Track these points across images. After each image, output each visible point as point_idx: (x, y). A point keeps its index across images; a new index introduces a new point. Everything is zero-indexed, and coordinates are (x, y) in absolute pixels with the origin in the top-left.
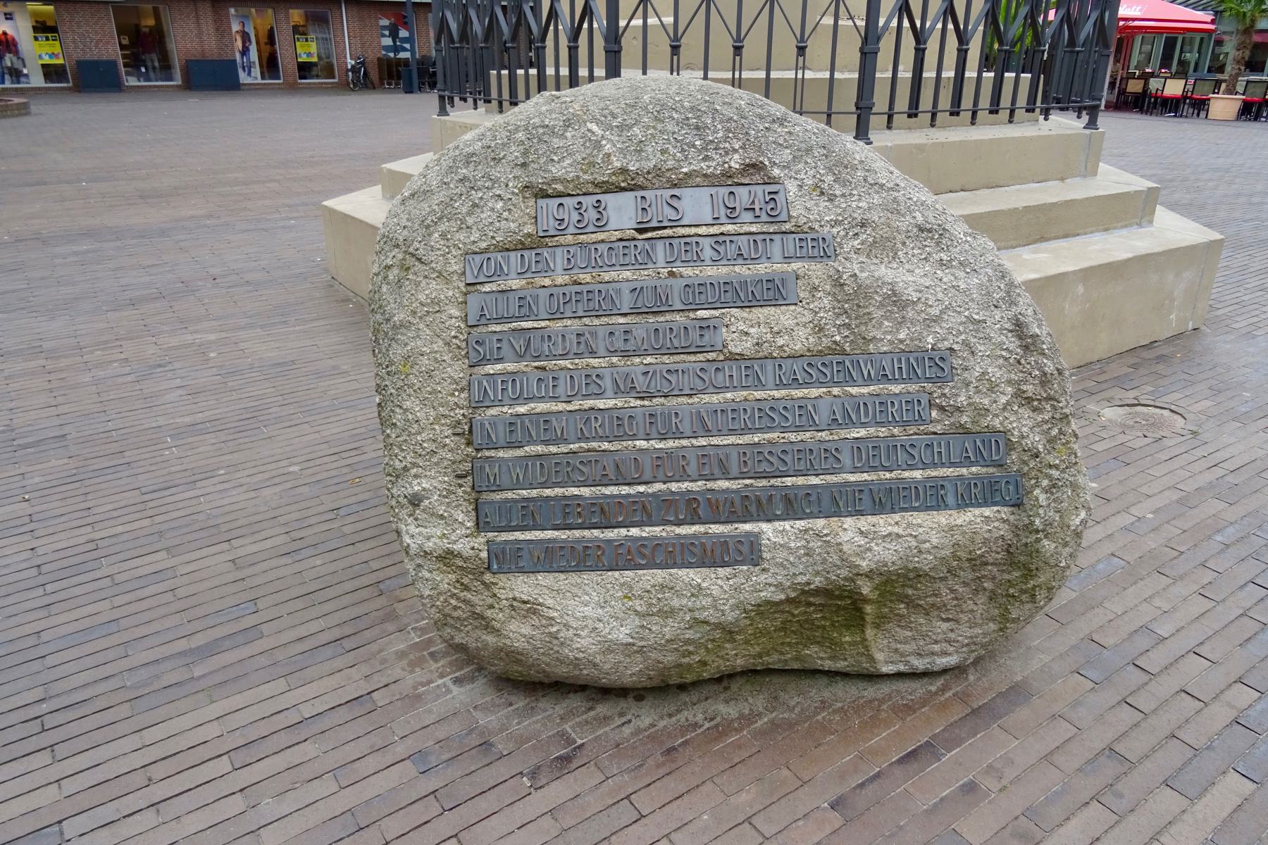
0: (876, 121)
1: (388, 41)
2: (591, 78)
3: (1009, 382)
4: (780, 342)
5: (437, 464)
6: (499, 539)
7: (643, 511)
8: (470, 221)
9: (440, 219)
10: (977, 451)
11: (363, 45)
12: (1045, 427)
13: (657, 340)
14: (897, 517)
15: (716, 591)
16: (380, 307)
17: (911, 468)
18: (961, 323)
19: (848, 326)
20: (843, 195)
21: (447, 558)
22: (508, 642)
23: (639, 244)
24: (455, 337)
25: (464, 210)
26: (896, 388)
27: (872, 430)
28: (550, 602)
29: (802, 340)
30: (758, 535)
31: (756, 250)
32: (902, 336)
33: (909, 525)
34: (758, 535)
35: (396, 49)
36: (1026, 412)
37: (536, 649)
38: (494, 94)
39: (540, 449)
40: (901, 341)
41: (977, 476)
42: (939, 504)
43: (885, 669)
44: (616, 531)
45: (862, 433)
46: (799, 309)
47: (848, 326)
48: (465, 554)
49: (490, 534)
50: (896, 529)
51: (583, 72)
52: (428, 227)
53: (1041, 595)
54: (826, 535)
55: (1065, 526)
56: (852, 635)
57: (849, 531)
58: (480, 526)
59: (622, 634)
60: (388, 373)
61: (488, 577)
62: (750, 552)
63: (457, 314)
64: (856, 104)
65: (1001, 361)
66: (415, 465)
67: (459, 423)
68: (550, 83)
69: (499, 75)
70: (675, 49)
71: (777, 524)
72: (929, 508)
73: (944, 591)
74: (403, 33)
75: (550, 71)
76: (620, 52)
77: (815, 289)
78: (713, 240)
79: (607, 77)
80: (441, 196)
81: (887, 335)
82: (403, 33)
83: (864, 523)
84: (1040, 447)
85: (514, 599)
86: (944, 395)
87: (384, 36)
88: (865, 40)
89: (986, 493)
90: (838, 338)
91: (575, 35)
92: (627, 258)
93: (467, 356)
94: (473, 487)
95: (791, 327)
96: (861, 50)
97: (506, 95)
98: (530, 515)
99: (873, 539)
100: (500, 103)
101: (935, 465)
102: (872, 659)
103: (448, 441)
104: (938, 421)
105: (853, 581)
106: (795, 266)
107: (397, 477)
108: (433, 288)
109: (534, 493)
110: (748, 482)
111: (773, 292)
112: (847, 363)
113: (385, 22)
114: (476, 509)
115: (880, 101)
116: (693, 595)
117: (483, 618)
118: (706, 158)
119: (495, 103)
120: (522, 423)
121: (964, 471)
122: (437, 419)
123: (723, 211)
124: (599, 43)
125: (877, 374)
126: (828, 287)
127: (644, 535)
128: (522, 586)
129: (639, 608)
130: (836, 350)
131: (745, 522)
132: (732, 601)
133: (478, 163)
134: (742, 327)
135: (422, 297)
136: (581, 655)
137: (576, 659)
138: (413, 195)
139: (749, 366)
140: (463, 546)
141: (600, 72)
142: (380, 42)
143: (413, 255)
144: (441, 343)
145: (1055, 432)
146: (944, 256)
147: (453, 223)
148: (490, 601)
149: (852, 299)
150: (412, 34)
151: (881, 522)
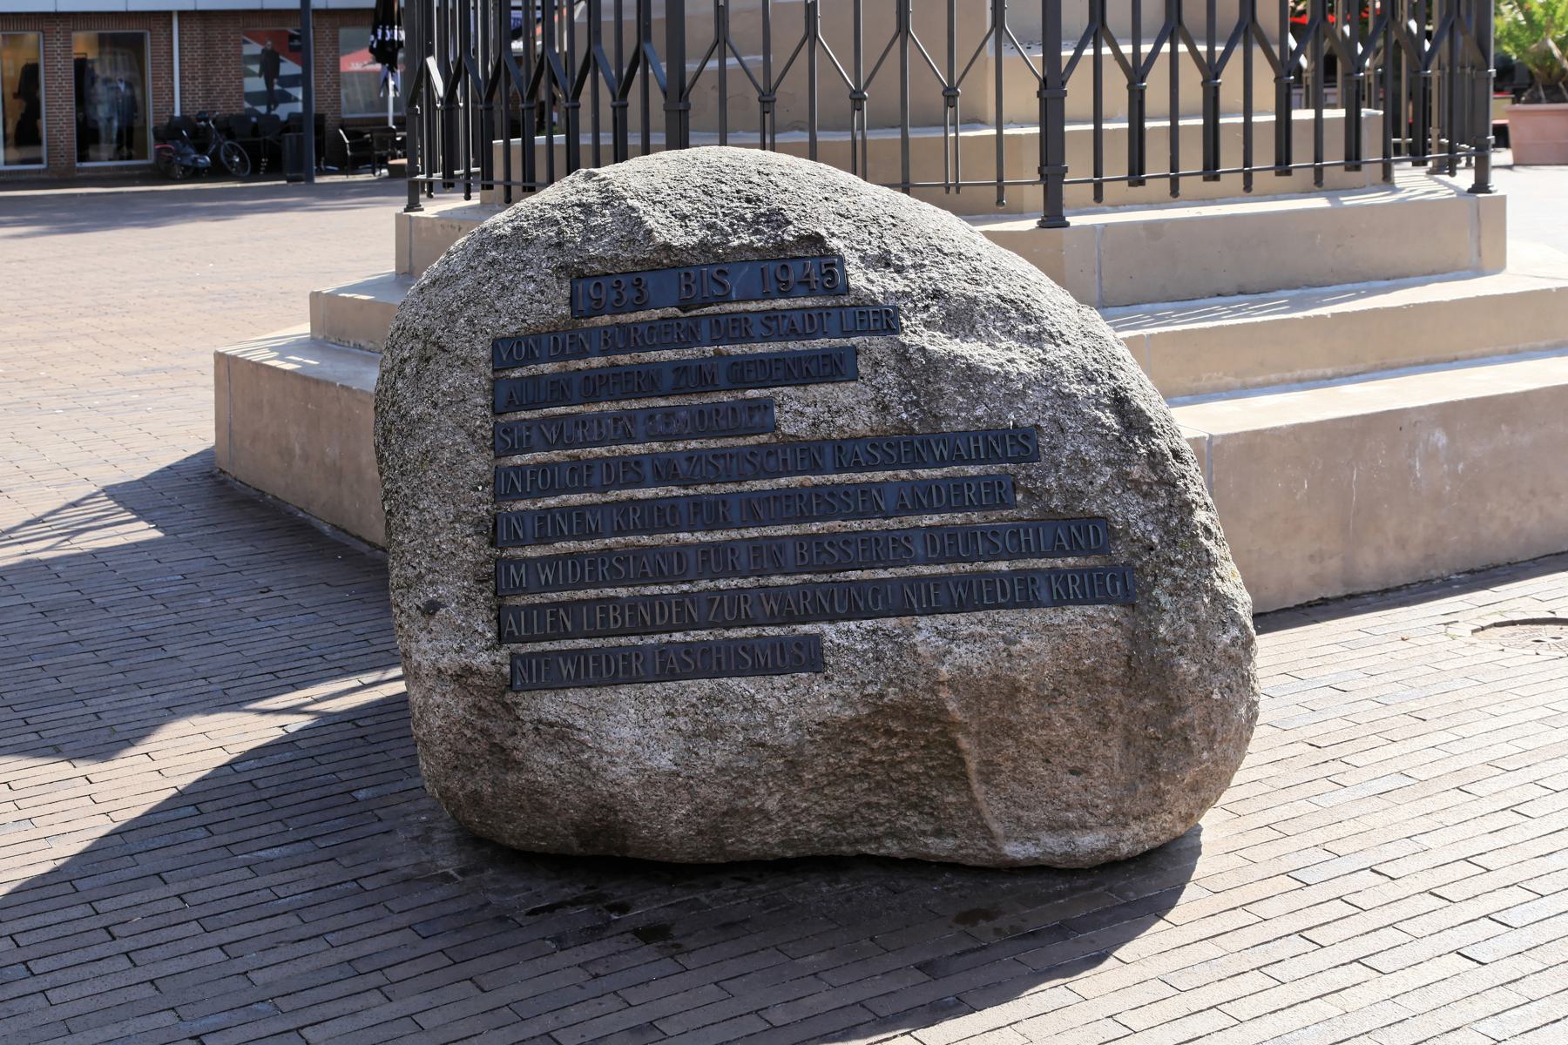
0: (1074, 191)
1: (256, 84)
2: (646, 150)
3: (1108, 462)
4: (840, 421)
5: (456, 568)
6: (523, 651)
7: (684, 613)
8: (499, 305)
9: (466, 304)
10: (1072, 540)
11: (208, 91)
12: (1161, 517)
13: (702, 423)
14: (981, 615)
15: (772, 704)
16: (393, 404)
17: (996, 559)
18: (1048, 398)
19: (916, 404)
20: (913, 266)
21: (463, 676)
22: (531, 777)
23: (683, 323)
24: (480, 427)
25: (493, 294)
26: (972, 470)
27: (947, 516)
28: (581, 723)
29: (863, 422)
30: (817, 638)
31: (812, 326)
32: (979, 412)
33: (995, 624)
34: (817, 638)
35: (272, 98)
36: (1133, 498)
37: (563, 783)
38: (498, 173)
39: (572, 546)
40: (978, 419)
41: (1074, 570)
42: (1029, 602)
43: (1015, 850)
44: (657, 637)
45: (935, 519)
46: (859, 386)
47: (916, 404)
48: (484, 669)
49: (514, 646)
50: (979, 629)
51: (634, 140)
52: (452, 313)
53: (1197, 740)
54: (898, 635)
55: (1208, 645)
56: (957, 792)
57: (926, 632)
58: (501, 638)
59: (665, 761)
60: (402, 474)
61: (509, 697)
62: (810, 657)
63: (483, 402)
64: (1040, 171)
65: (1097, 438)
66: (430, 570)
67: (482, 520)
68: (586, 155)
69: (507, 146)
70: (767, 100)
71: (841, 624)
72: (1016, 606)
73: (1059, 722)
74: (289, 68)
75: (585, 140)
76: (686, 111)
77: (877, 363)
78: (762, 317)
79: (669, 147)
80: (468, 281)
81: (960, 413)
82: (289, 68)
83: (941, 621)
84: (1155, 539)
85: (540, 721)
86: (1029, 476)
87: (252, 74)
88: (1044, 82)
89: (1089, 588)
90: (904, 416)
91: (621, 91)
92: (669, 339)
93: (493, 447)
94: (495, 593)
95: (848, 408)
96: (1039, 94)
97: (517, 175)
98: (557, 621)
99: (953, 640)
100: (508, 190)
101: (1021, 556)
102: (989, 834)
103: (469, 540)
104: (1025, 507)
105: (934, 692)
106: (854, 340)
107: (409, 586)
108: (456, 378)
109: (565, 596)
110: (806, 577)
111: (836, 368)
112: (917, 444)
113: (254, 49)
114: (498, 618)
115: (1078, 165)
116: (745, 709)
117: (503, 750)
118: (757, 232)
119: (499, 190)
120: (553, 518)
121: (1059, 562)
122: (457, 519)
123: (774, 286)
124: (657, 99)
125: (950, 456)
126: (892, 362)
127: (688, 639)
128: (549, 706)
129: (683, 727)
130: (904, 429)
131: (804, 623)
132: (792, 717)
133: (507, 246)
134: (796, 406)
135: (444, 387)
136: (617, 789)
137: (611, 795)
138: (433, 283)
139: (809, 454)
140: (483, 660)
141: (658, 138)
142: (241, 86)
143: (434, 344)
144: (464, 434)
145: (1174, 522)
146: (1032, 328)
147: (480, 308)
148: (511, 725)
149: (924, 372)
150: (306, 66)
151: (963, 621)
